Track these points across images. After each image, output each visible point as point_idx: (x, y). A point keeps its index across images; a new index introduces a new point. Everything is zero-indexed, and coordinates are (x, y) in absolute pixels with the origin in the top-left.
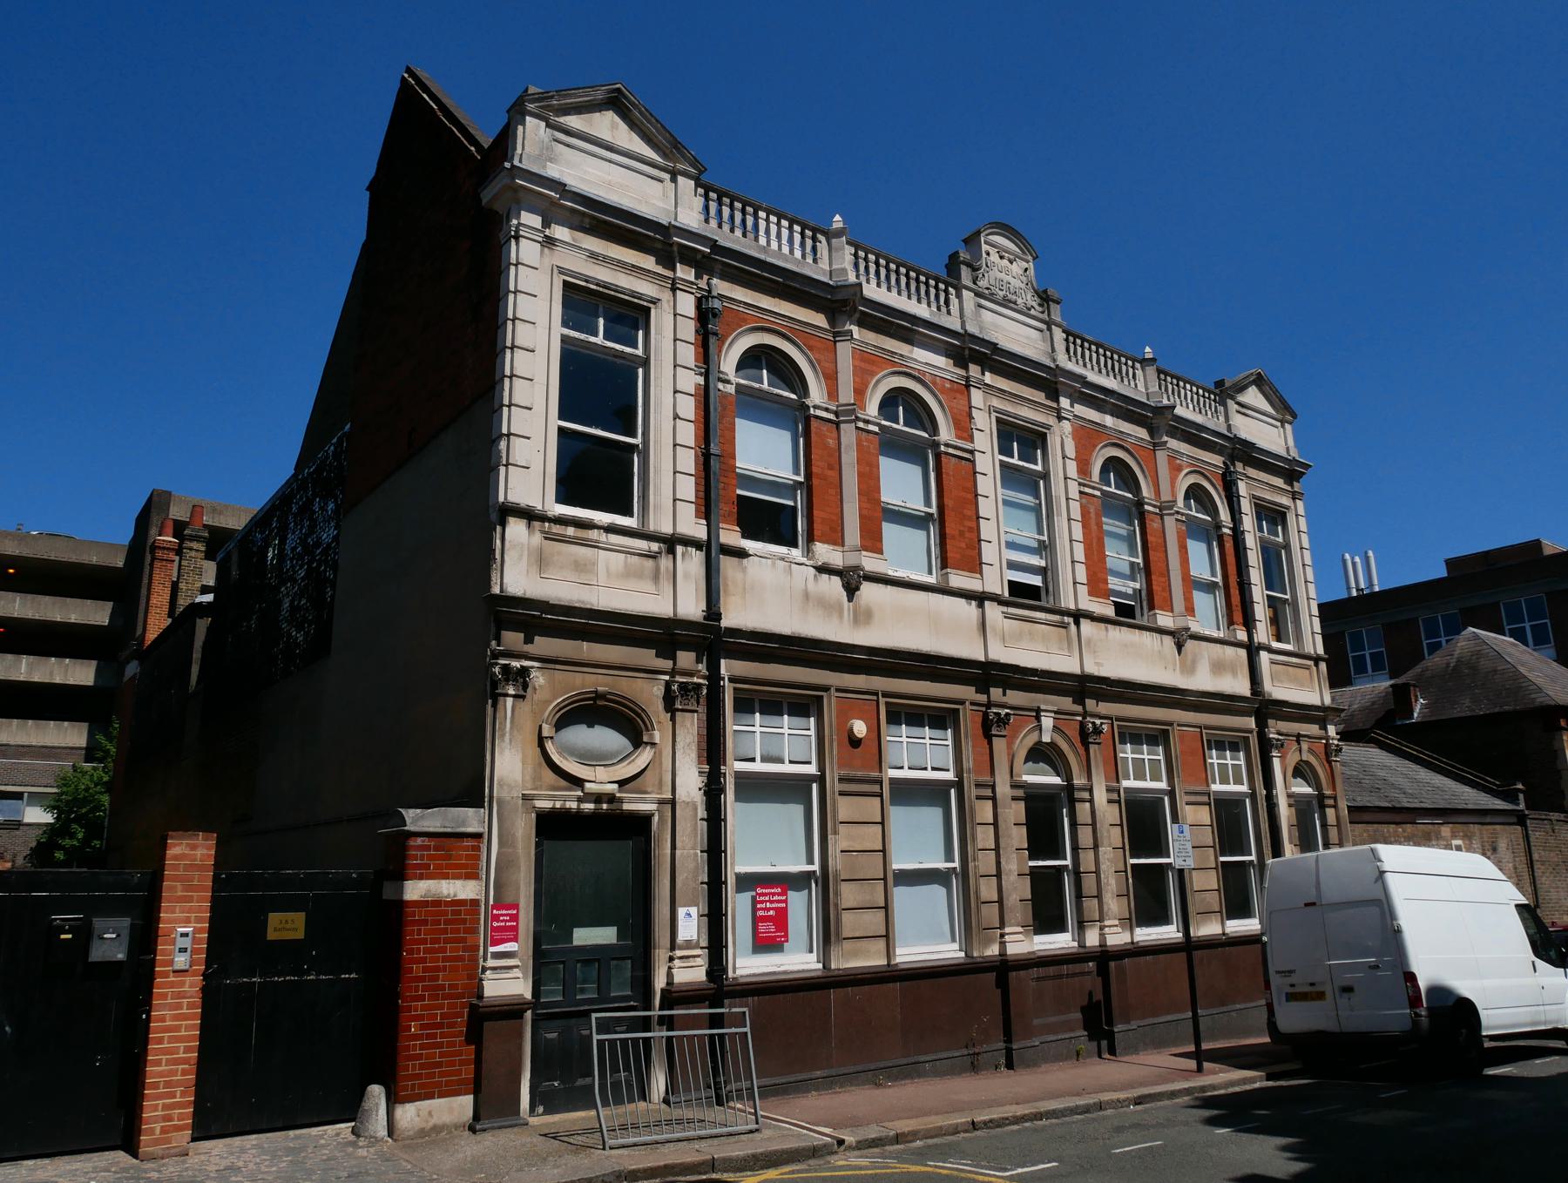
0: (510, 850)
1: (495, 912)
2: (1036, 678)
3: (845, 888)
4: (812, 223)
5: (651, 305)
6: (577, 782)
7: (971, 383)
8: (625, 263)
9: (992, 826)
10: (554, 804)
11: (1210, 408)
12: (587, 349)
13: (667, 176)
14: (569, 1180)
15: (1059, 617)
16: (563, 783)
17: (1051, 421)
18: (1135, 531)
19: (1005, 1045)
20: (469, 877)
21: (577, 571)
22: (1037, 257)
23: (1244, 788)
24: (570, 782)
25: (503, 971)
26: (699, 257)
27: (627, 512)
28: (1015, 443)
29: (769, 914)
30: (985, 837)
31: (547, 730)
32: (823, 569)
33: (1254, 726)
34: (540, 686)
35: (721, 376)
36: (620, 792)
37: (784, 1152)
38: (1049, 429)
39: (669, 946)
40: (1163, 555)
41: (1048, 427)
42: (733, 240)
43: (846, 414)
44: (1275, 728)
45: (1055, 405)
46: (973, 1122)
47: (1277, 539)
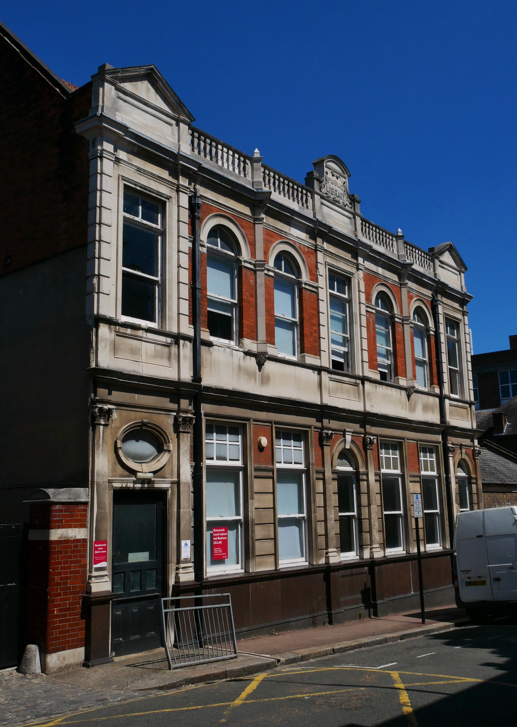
0: (103, 511)
1: (96, 545)
2: (344, 414)
3: (257, 529)
4: (244, 153)
5: (167, 200)
6: (133, 472)
7: (318, 249)
8: (154, 175)
9: (322, 494)
10: (122, 485)
11: (427, 264)
12: (135, 225)
13: (174, 122)
14: (164, 684)
15: (354, 380)
16: (126, 473)
17: (354, 270)
18: (389, 332)
19: (327, 611)
21: (131, 353)
22: (350, 176)
23: (435, 473)
24: (130, 473)
26: (191, 172)
27: (152, 319)
28: (336, 282)
30: (319, 500)
32: (248, 353)
33: (441, 440)
34: (115, 419)
35: (201, 243)
36: (154, 477)
38: (352, 275)
39: (176, 561)
40: (402, 346)
41: (352, 274)
42: (207, 163)
43: (260, 265)
44: (452, 440)
45: (355, 261)
46: (333, 650)
47: (454, 337)
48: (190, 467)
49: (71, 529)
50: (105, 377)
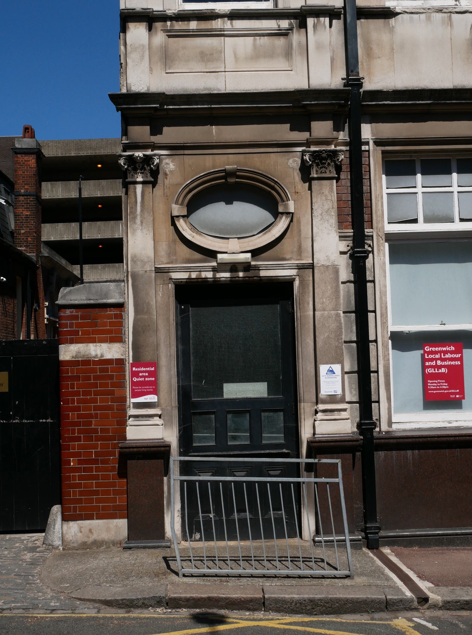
1: (134, 369)
10: (190, 275)
16: (198, 256)
20: (113, 340)
25: (144, 419)
29: (440, 371)
31: (177, 210)
34: (171, 172)
37: (348, 601)
48: (337, 238)
49: (95, 344)
50: (133, 106)
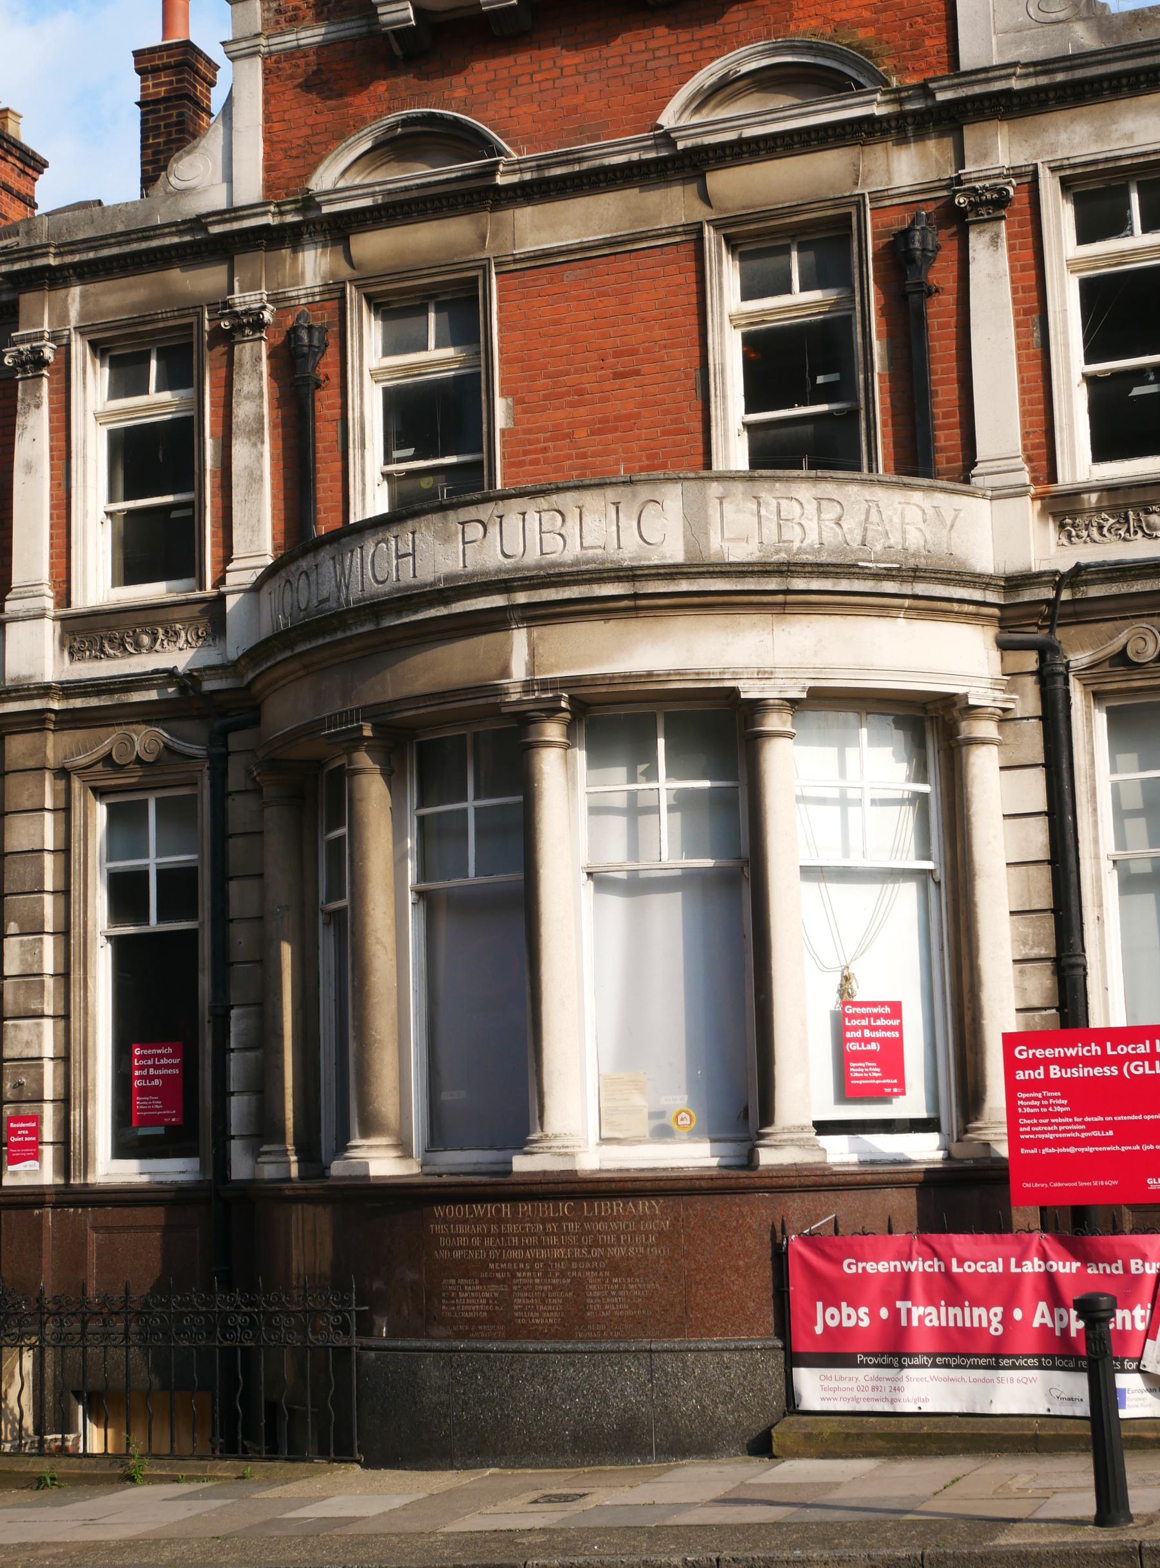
1: (12, 1125)
29: (869, 1047)
